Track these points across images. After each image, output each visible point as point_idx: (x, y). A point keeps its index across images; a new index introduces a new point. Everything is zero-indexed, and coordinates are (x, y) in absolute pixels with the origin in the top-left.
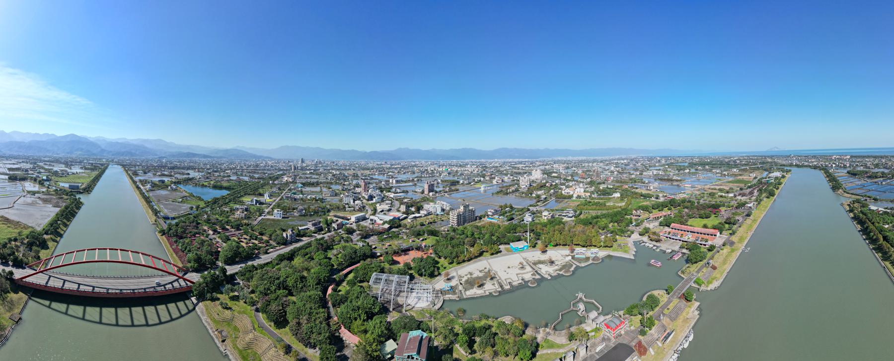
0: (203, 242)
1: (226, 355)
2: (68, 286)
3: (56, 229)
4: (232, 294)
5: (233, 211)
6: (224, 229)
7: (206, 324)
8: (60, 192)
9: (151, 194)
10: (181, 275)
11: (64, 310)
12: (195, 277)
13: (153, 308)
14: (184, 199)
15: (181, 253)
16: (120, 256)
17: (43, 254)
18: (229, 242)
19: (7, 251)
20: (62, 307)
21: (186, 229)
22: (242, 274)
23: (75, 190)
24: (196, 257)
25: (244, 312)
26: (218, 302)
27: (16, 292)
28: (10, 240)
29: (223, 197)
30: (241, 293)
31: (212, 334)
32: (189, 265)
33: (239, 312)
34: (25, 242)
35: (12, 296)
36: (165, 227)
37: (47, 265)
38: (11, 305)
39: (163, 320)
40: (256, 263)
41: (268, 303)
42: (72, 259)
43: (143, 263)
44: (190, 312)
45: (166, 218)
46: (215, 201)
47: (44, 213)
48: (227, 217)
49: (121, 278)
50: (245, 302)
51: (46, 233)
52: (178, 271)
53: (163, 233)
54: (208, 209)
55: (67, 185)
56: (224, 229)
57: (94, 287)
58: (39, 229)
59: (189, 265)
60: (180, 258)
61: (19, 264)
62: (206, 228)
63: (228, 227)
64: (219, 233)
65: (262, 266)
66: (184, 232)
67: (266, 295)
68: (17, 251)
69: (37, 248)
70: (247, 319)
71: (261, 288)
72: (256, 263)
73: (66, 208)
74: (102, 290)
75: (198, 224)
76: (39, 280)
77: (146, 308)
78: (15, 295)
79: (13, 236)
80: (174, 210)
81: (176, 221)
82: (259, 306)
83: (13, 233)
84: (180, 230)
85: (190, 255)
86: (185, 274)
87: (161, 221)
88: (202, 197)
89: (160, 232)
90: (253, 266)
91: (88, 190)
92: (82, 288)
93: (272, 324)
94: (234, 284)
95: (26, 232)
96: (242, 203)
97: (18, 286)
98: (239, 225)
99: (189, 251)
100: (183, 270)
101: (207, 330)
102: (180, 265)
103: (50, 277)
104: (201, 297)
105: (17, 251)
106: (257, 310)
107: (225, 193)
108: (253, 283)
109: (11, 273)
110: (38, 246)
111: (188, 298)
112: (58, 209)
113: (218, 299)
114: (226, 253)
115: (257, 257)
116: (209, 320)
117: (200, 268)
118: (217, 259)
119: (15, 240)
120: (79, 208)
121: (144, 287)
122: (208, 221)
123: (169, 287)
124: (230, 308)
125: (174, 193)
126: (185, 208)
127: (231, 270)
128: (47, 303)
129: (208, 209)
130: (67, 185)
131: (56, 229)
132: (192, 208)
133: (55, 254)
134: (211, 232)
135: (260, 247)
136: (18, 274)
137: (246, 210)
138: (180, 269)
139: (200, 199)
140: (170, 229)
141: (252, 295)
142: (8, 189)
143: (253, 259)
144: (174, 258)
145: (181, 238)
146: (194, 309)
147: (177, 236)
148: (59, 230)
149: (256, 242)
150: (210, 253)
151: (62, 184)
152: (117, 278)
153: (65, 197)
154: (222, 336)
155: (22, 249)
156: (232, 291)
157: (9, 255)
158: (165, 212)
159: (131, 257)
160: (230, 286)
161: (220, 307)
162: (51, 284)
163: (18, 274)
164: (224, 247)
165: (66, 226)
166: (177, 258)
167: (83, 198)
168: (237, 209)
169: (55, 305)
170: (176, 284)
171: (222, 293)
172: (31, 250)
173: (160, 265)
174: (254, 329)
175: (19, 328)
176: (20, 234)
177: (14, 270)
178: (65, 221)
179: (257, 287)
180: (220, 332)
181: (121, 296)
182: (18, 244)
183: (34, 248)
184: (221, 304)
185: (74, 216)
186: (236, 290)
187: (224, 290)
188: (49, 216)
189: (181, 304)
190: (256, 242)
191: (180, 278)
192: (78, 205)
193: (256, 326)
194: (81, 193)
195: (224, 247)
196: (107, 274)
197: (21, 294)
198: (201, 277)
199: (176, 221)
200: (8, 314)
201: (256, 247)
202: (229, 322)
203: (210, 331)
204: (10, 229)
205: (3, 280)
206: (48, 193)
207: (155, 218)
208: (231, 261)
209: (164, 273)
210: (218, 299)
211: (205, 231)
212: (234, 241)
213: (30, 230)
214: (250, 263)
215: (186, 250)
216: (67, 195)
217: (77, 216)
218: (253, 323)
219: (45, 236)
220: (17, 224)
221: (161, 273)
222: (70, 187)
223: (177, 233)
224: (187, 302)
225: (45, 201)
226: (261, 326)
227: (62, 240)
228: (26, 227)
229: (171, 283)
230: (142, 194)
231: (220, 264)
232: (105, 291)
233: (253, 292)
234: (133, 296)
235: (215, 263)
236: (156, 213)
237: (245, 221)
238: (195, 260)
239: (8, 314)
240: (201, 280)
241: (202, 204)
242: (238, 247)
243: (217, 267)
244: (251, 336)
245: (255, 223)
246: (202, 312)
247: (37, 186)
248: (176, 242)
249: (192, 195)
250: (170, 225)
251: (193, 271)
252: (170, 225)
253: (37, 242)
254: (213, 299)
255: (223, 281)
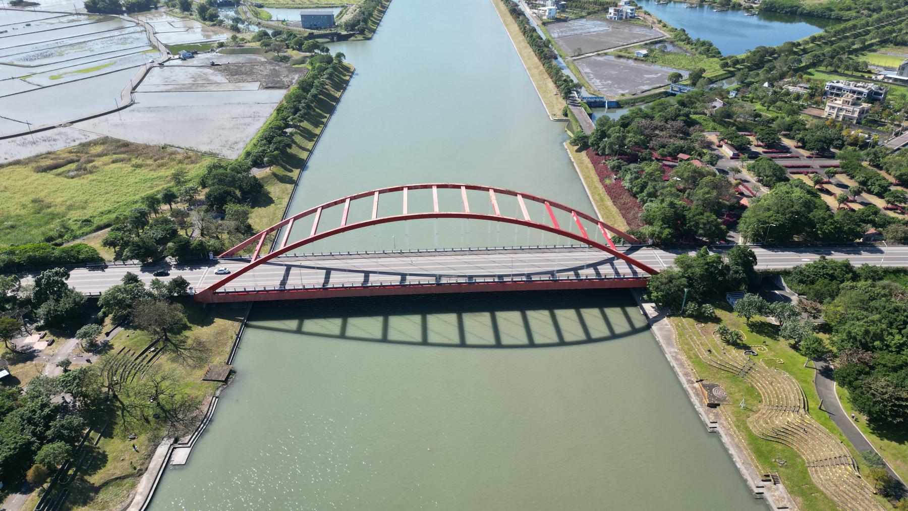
0: (696, 177)
1: (714, 433)
2: (336, 280)
3: (283, 149)
4: (757, 318)
5: (817, 95)
6: (774, 146)
7: (673, 363)
8: (275, 41)
9: (555, 33)
10: (621, 250)
11: (337, 331)
12: (660, 260)
13: (546, 313)
14: (656, 49)
15: (627, 198)
16: (466, 202)
17: (260, 219)
18: (782, 187)
19: (150, 233)
20: (333, 325)
21: (649, 138)
22: (803, 278)
23: (320, 30)
24: (669, 212)
25: (784, 366)
26: (713, 327)
27: (205, 321)
28: (153, 202)
29: (792, 49)
30: (788, 324)
31: (686, 385)
32: (646, 230)
33: (770, 363)
34: (201, 196)
35: (198, 333)
36: (590, 127)
37: (275, 242)
38: (202, 351)
39: (568, 338)
40: (858, 261)
41: (868, 369)
42: (340, 217)
43: (527, 218)
44: (635, 331)
45: (595, 104)
46: (762, 59)
47: (238, 111)
48: (794, 112)
49: (471, 251)
50: (795, 347)
51: (258, 163)
52: (615, 241)
53: (582, 143)
54: (730, 86)
55: (294, 17)
56: (774, 146)
57: (404, 276)
58: (233, 156)
59: (646, 230)
60: (624, 210)
61: (196, 256)
62: (713, 137)
63: (786, 142)
64: (754, 156)
65: (876, 275)
66: (644, 144)
67: (866, 347)
68: (183, 225)
69: (238, 207)
70: (784, 384)
71: (858, 329)
72: (858, 261)
73: (305, 87)
74: (424, 281)
75: (690, 123)
76: (263, 279)
77: (530, 314)
78: (205, 329)
79: (159, 189)
80: (619, 81)
81: (625, 112)
82: (835, 365)
83: (157, 179)
84: (631, 138)
85: (653, 206)
86: (634, 249)
87: (581, 113)
88: (718, 42)
89: (574, 143)
90: (848, 267)
91: (363, 27)
92: (374, 280)
93: (864, 418)
94: (773, 298)
95: (196, 171)
96: (862, 72)
97: (207, 307)
98: (830, 142)
99: (653, 195)
100: (630, 241)
101: (675, 375)
102: (623, 227)
103: (289, 268)
104: (671, 305)
105: (183, 225)
106: (827, 373)
107: (802, 32)
108: (830, 310)
109: (181, 284)
110: (239, 201)
111: (635, 304)
112: (278, 96)
113: (717, 320)
114: (763, 215)
115: (870, 245)
116: (684, 358)
117: (678, 235)
118: (733, 226)
119: (169, 198)
120: (342, 85)
121: (527, 271)
122: (724, 118)
123: (589, 273)
124: (746, 348)
125: (626, 30)
126: (654, 77)
127: (768, 260)
128: (293, 324)
129: (730, 86)
130: (294, 17)
131: (283, 149)
132: (677, 78)
133: (292, 214)
134: (727, 151)
135: (891, 221)
136: (200, 280)
137: (872, 97)
138: (620, 237)
139: (709, 50)
140: (603, 135)
141: (821, 335)
142: (98, 47)
143: (855, 249)
144: (607, 211)
145: (633, 159)
146: (648, 327)
147: (621, 153)
148: (294, 150)
149: (880, 203)
150: (717, 208)
151: (278, 15)
152: (462, 252)
153: (295, 55)
154: (711, 395)
155: (194, 217)
156: (760, 310)
157: (163, 241)
158: (596, 85)
159: (495, 204)
160: (756, 298)
161: (717, 339)
162: (292, 283)
163: (200, 280)
164: (758, 196)
165: (311, 136)
166: (614, 210)
167: (350, 53)
168: (838, 92)
169: (310, 325)
170: (606, 271)
171: (731, 310)
172: (222, 215)
173: (569, 223)
174: (807, 409)
175: (234, 390)
176: (178, 178)
177: (187, 274)
178: (305, 124)
179: (843, 321)
180: (710, 388)
181: (471, 290)
182: (182, 206)
183: (231, 208)
184: (723, 332)
185: (331, 110)
186: (772, 312)
187: (736, 303)
188: (255, 117)
189: (615, 314)
190: (880, 203)
191: (618, 256)
192: (339, 75)
193: (812, 405)
194: (342, 38)
195: (758, 196)
196: (437, 244)
197: (219, 323)
198: (677, 262)
199: (625, 112)
200: (200, 373)
201: (871, 216)
202: (738, 374)
203: (683, 380)
204: (144, 173)
205: (163, 305)
206: (238, 48)
207: (563, 104)
208: (776, 237)
209: (577, 243)
210: (717, 320)
211: (709, 145)
212: (801, 185)
213: (207, 162)
214: (838, 257)
215: (642, 190)
216: (299, 47)
217: (340, 108)
218: (805, 394)
219: (257, 173)
220: (161, 154)
221: (569, 241)
222: (308, 21)
223: (623, 145)
224: (631, 310)
225: (235, 73)
226: (827, 410)
227: (306, 174)
228: (193, 156)
229: (594, 266)
230: (529, 32)
231: (740, 241)
232: (432, 281)
233: (826, 328)
234: (499, 289)
235: (722, 236)
236: (567, 89)
237: (859, 133)
238: (666, 220)
239: (200, 373)
240: (677, 269)
241: (712, 67)
242: (809, 206)
243: (728, 245)
244: (792, 418)
245: (895, 143)
246: (668, 339)
247: (198, 25)
248: (617, 169)
249: (682, 37)
250: (604, 122)
251: (655, 246)
252: (604, 123)
253: (235, 191)
254: (701, 318)
255: (738, 282)
